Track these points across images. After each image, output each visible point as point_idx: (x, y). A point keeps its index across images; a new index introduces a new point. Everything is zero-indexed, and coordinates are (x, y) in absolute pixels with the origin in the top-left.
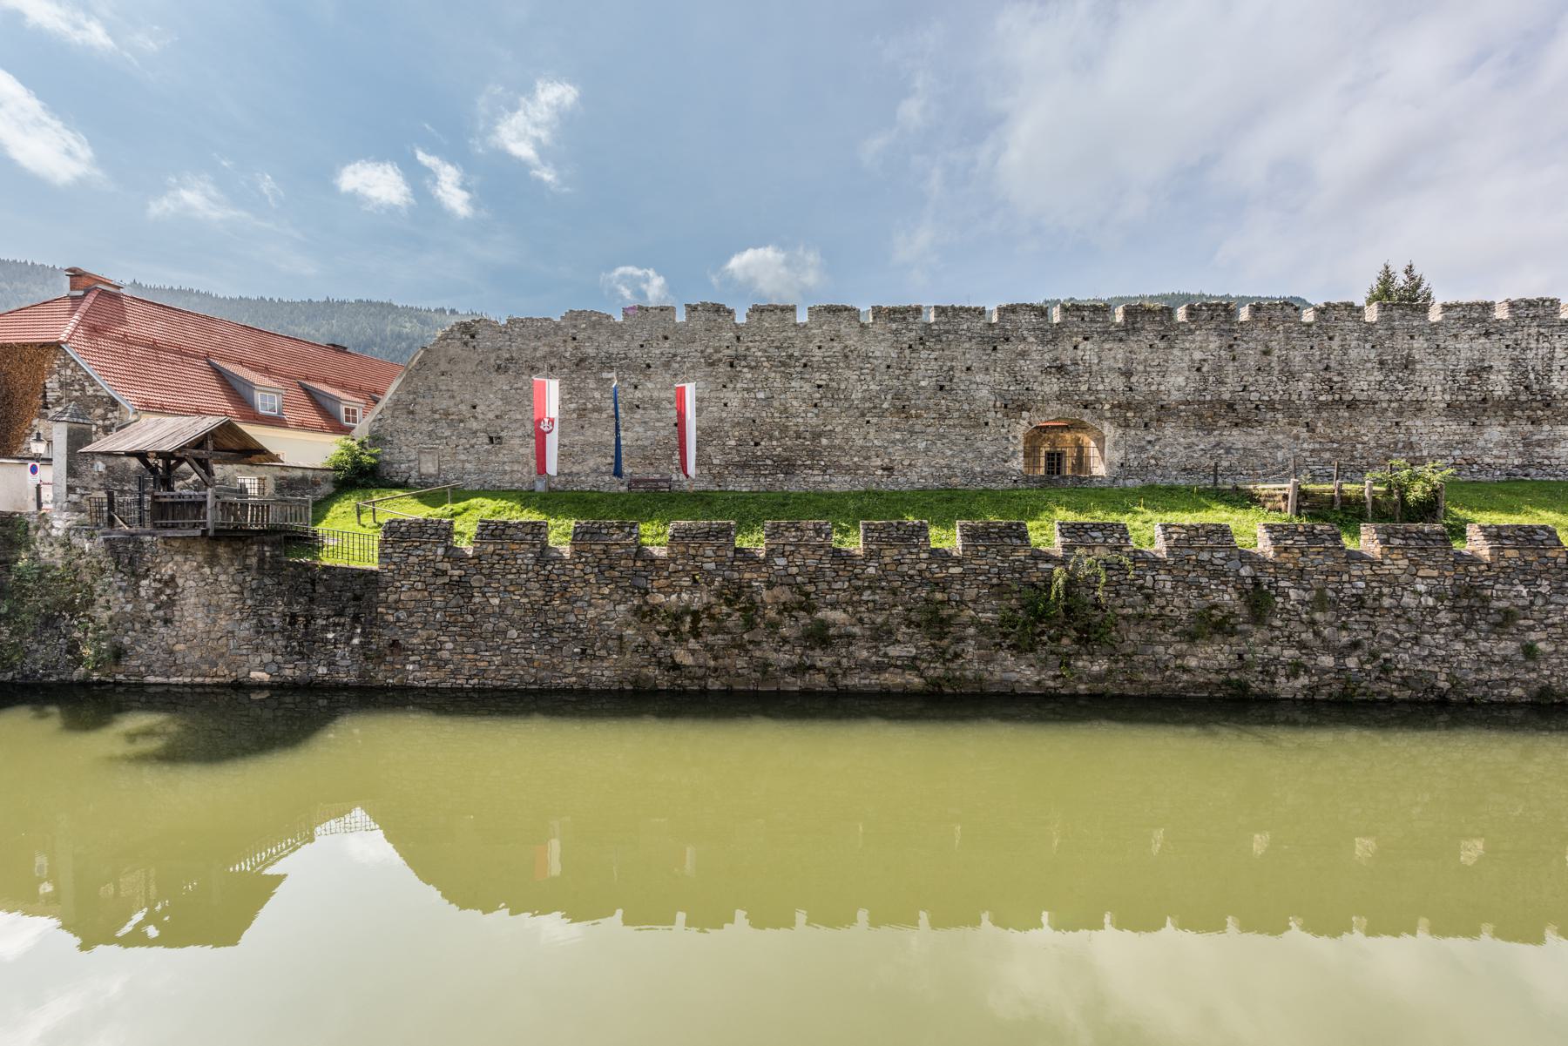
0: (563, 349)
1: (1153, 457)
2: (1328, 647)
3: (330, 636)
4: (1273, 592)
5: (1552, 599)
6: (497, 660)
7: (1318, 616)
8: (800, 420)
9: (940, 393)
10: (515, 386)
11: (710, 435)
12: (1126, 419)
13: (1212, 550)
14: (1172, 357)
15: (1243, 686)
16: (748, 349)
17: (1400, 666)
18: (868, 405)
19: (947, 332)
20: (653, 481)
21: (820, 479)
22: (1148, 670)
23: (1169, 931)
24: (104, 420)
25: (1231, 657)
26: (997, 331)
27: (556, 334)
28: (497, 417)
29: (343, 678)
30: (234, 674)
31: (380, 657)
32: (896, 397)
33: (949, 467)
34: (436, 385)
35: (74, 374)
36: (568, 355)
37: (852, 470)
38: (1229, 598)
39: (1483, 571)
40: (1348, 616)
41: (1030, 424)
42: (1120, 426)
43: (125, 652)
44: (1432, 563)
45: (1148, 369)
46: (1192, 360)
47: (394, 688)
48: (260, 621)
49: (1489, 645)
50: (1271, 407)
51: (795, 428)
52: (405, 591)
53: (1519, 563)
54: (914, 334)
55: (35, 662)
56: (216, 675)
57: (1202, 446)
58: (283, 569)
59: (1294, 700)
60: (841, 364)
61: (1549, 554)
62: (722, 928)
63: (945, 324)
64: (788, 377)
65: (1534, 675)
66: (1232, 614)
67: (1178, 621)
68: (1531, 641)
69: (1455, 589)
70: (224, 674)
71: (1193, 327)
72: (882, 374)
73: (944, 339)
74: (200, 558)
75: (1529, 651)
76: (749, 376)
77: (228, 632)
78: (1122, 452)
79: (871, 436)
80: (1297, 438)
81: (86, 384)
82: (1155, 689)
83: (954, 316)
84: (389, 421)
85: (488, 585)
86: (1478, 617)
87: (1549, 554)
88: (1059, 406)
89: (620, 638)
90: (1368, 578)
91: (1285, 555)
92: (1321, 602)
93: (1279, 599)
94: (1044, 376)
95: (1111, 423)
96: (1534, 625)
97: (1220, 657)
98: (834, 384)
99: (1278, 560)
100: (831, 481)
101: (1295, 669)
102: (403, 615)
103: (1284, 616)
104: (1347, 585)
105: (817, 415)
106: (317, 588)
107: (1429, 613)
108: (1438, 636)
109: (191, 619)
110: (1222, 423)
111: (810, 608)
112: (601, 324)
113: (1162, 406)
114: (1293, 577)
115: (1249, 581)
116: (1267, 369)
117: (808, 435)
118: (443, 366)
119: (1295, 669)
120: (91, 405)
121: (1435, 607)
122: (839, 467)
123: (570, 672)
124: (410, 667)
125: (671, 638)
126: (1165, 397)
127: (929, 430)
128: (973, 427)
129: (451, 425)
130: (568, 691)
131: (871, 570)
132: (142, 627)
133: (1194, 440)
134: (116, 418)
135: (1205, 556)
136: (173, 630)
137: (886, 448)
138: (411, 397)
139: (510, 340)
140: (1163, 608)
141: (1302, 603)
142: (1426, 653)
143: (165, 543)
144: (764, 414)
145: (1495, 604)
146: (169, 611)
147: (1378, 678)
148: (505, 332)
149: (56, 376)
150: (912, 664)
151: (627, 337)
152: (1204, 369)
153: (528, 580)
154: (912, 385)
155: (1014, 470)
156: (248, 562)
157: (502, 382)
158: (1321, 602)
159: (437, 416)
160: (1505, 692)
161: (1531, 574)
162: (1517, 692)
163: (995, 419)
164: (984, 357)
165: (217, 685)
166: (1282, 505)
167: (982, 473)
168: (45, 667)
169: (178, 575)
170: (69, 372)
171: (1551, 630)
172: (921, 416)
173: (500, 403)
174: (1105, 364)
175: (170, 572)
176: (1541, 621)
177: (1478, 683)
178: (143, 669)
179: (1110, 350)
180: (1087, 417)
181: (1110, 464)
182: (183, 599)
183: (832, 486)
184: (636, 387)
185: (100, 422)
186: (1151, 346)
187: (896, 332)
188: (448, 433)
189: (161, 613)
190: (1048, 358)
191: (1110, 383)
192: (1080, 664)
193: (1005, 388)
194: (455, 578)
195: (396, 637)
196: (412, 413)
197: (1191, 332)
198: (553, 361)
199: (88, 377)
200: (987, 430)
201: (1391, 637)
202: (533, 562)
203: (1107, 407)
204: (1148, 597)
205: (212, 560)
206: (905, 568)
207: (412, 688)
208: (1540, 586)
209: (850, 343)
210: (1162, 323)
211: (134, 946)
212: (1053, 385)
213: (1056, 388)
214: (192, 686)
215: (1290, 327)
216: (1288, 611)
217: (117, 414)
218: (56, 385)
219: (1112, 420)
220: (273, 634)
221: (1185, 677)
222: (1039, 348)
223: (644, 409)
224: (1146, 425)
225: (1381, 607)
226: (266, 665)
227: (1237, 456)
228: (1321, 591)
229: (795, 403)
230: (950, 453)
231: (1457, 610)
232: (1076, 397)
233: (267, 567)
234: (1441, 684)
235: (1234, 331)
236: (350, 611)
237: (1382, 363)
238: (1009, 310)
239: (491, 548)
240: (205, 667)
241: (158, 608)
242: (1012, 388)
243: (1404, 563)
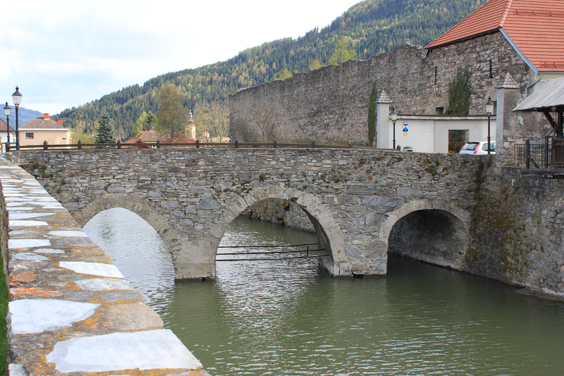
81: (512, 56)
134: (527, 80)
170: (503, 49)
199: (513, 50)
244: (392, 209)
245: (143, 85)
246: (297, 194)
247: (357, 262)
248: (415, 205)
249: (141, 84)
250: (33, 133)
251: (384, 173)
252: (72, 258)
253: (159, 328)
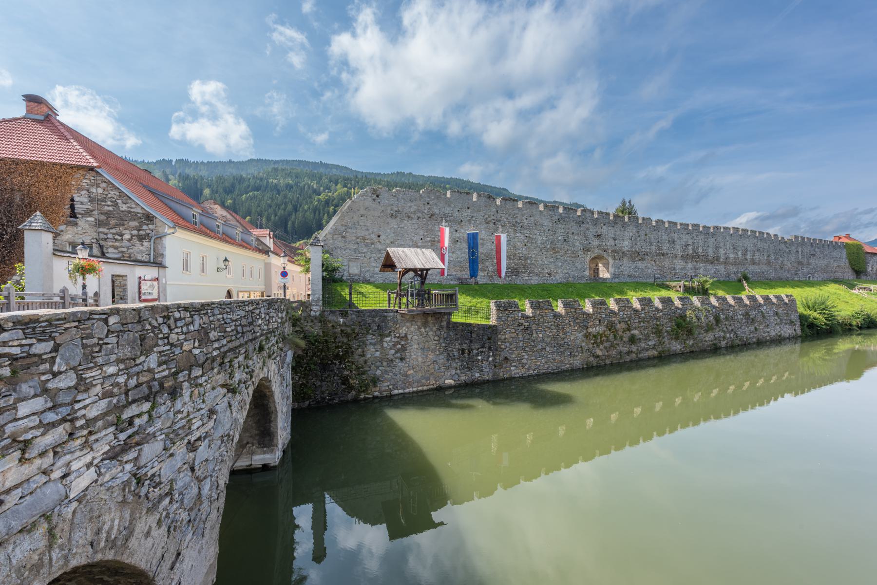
0: (423, 208)
3: (480, 358)
6: (543, 361)
10: (401, 226)
11: (487, 257)
16: (501, 217)
19: (567, 217)
20: (465, 279)
21: (527, 278)
23: (627, 448)
24: (139, 231)
27: (420, 200)
28: (391, 242)
29: (486, 377)
30: (438, 383)
31: (501, 366)
33: (568, 273)
34: (358, 222)
35: (106, 193)
36: (426, 212)
37: (537, 275)
43: (378, 379)
47: (507, 379)
48: (448, 354)
52: (507, 334)
55: (323, 393)
56: (429, 385)
58: (458, 327)
62: (325, 548)
64: (515, 231)
70: (433, 383)
74: (419, 324)
77: (434, 361)
79: (544, 260)
81: (119, 201)
84: (330, 242)
85: (538, 329)
89: (581, 347)
100: (531, 279)
102: (508, 345)
106: (473, 335)
109: (415, 357)
110: (637, 259)
112: (441, 197)
117: (523, 258)
118: (362, 212)
120: (124, 218)
123: (568, 362)
124: (513, 368)
125: (595, 345)
127: (562, 258)
129: (367, 245)
130: (566, 371)
131: (643, 315)
132: (388, 364)
136: (406, 363)
138: (344, 228)
139: (398, 200)
143: (402, 316)
146: (403, 354)
148: (395, 196)
149: (84, 192)
151: (452, 205)
153: (551, 325)
156: (442, 324)
157: (394, 223)
159: (358, 240)
165: (429, 390)
166: (679, 289)
168: (330, 394)
169: (408, 333)
170: (100, 190)
173: (393, 235)
175: (404, 332)
178: (391, 387)
180: (605, 255)
181: (611, 274)
182: (410, 346)
184: (456, 231)
185: (135, 232)
187: (551, 215)
188: (365, 250)
189: (399, 355)
194: (526, 326)
195: (506, 356)
196: (344, 237)
198: (419, 214)
202: (552, 317)
205: (425, 324)
206: (650, 314)
207: (514, 378)
209: (536, 218)
214: (417, 392)
217: (151, 227)
218: (86, 200)
220: (455, 359)
223: (460, 242)
226: (453, 376)
229: (518, 244)
233: (451, 326)
236: (487, 345)
237: (669, 241)
239: (538, 312)
240: (424, 381)
241: (396, 352)
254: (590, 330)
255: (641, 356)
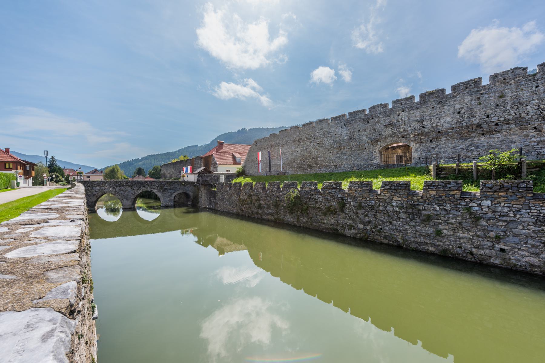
1: (434, 154)
2: (362, 222)
4: (346, 203)
5: (451, 212)
7: (359, 211)
8: (313, 154)
9: (350, 140)
12: (421, 139)
13: (332, 189)
14: (444, 110)
15: (336, 230)
16: (302, 136)
17: (385, 231)
18: (330, 147)
19: (353, 120)
21: (318, 170)
22: (315, 222)
25: (335, 221)
26: (369, 116)
32: (338, 143)
33: (353, 164)
38: (335, 204)
39: (419, 199)
40: (368, 212)
41: (381, 146)
42: (419, 143)
44: (398, 195)
45: (431, 117)
46: (455, 109)
49: (421, 228)
50: (507, 122)
51: (312, 156)
53: (436, 196)
54: (342, 123)
57: (461, 147)
59: (350, 237)
60: (323, 136)
61: (451, 193)
63: (351, 118)
65: (441, 244)
66: (335, 209)
67: (322, 209)
68: (441, 229)
69: (407, 205)
71: (455, 94)
72: (334, 137)
73: (351, 123)
75: (439, 233)
76: (302, 143)
78: (419, 153)
79: (331, 156)
80: (527, 136)
82: (316, 228)
83: (354, 115)
86: (416, 217)
87: (451, 193)
88: (391, 139)
90: (375, 200)
91: (350, 191)
92: (360, 206)
93: (348, 205)
94: (386, 129)
95: (414, 142)
96: (441, 223)
97: (332, 221)
98: (321, 142)
99: (348, 193)
100: (321, 171)
101: (351, 227)
103: (349, 210)
104: (368, 202)
105: (317, 152)
107: (396, 214)
108: (399, 222)
110: (473, 135)
111: (259, 201)
113: (439, 132)
114: (352, 198)
115: (340, 199)
116: (503, 104)
119: (351, 227)
121: (399, 212)
122: (323, 166)
126: (440, 128)
127: (347, 152)
128: (361, 150)
130: (231, 213)
131: (268, 193)
133: (456, 144)
135: (330, 191)
137: (335, 159)
140: (319, 205)
141: (355, 207)
142: (394, 228)
144: (305, 153)
145: (424, 212)
147: (377, 234)
150: (272, 215)
152: (462, 112)
154: (342, 139)
155: (375, 163)
158: (360, 206)
160: (426, 248)
161: (441, 201)
162: (432, 249)
163: (368, 146)
164: (364, 126)
167: (364, 165)
171: (450, 225)
172: (345, 148)
174: (411, 120)
176: (445, 221)
177: (415, 242)
179: (413, 113)
183: (321, 172)
186: (433, 108)
190: (387, 122)
191: (413, 127)
192: (301, 218)
193: (372, 135)
197: (454, 97)
200: (365, 150)
201: (382, 221)
203: (412, 136)
204: (316, 202)
208: (445, 206)
210: (438, 97)
211: (146, 220)
212: (389, 131)
213: (390, 132)
215: (519, 80)
216: (350, 209)
219: (414, 141)
221: (323, 225)
222: (384, 119)
224: (431, 141)
225: (379, 210)
227: (483, 149)
228: (360, 203)
229: (312, 149)
230: (353, 159)
231: (407, 213)
232: (399, 134)
234: (399, 240)
235: (480, 91)
238: (372, 108)
242: (374, 135)
243: (388, 195)
244: (174, 192)
245: (141, 159)
246: (152, 190)
247: (166, 203)
248: (180, 191)
249: (140, 158)
250: (26, 183)
251: (172, 185)
252: (339, 117)
253: (231, 164)
254: (241, 197)
255: (264, 217)
